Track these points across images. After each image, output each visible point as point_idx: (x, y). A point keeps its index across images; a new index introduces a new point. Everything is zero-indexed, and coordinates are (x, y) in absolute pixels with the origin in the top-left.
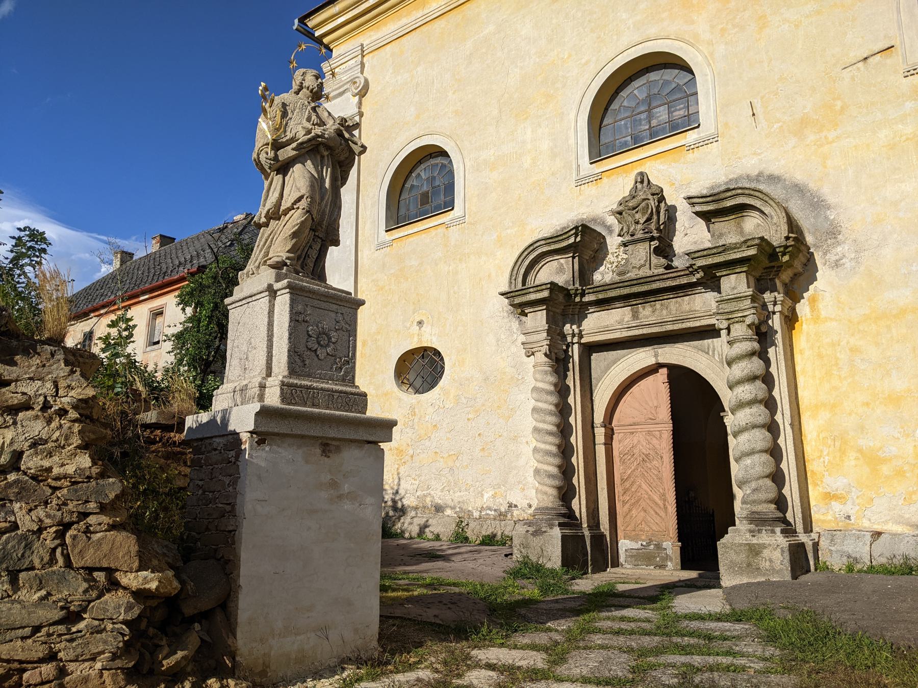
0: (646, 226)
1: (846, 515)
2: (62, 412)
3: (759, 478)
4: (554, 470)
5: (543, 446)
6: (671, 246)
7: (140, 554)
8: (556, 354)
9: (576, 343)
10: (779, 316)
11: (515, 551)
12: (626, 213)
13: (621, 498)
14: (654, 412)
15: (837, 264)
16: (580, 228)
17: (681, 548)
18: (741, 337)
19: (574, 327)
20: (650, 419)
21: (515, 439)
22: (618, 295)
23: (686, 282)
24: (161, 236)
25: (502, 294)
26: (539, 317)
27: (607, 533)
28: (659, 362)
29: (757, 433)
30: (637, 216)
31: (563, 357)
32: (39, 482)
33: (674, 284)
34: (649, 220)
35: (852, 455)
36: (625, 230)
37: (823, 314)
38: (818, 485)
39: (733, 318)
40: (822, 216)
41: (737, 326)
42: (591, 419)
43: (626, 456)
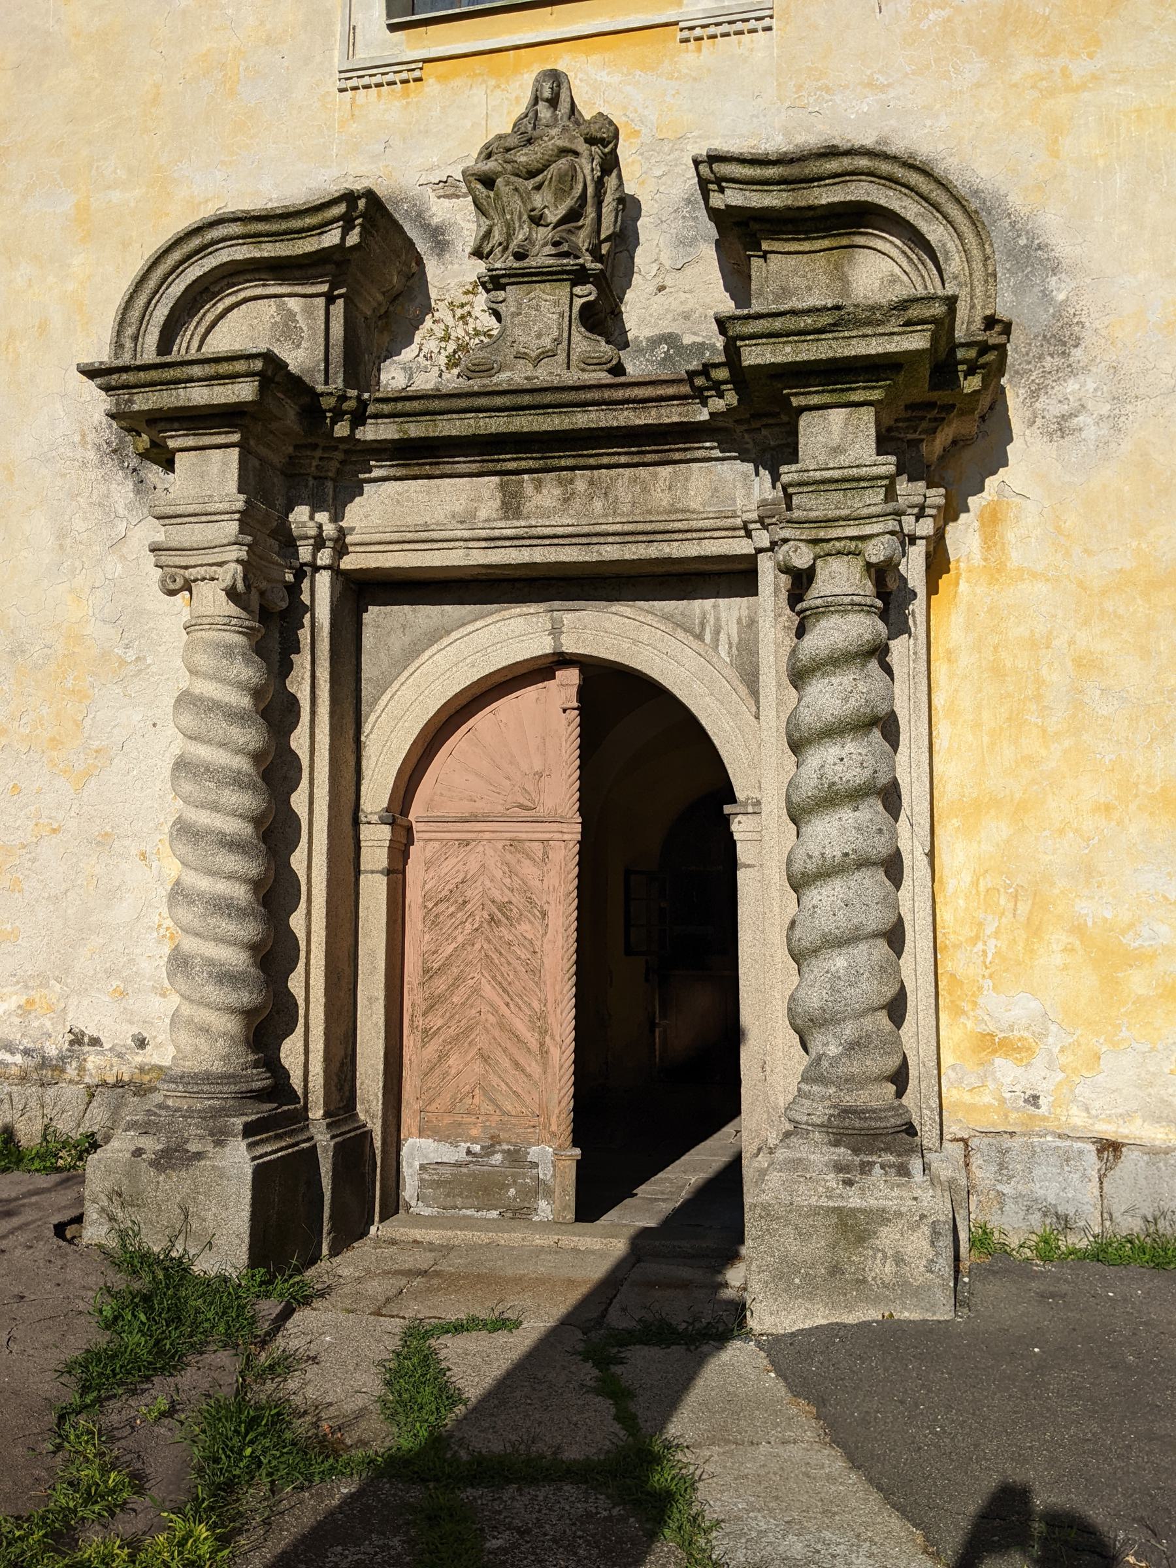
0: (564, 235)
1: (1029, 1092)
3: (865, 1013)
4: (236, 958)
5: (204, 884)
6: (617, 314)
8: (262, 594)
9: (325, 568)
10: (923, 549)
11: (92, 1213)
12: (508, 183)
13: (420, 1022)
14: (530, 787)
15: (1062, 428)
16: (361, 204)
17: (579, 1164)
18: (847, 600)
19: (322, 517)
20: (521, 806)
21: (103, 842)
22: (471, 432)
23: (675, 419)
25: (91, 373)
26: (214, 468)
27: (376, 1127)
28: (564, 649)
29: (868, 883)
30: (538, 200)
31: (284, 605)
33: (642, 422)
34: (573, 215)
35: (1058, 938)
36: (497, 236)
37: (1015, 558)
38: (964, 1012)
39: (828, 541)
40: (1036, 289)
41: (837, 565)
42: (353, 797)
43: (442, 907)
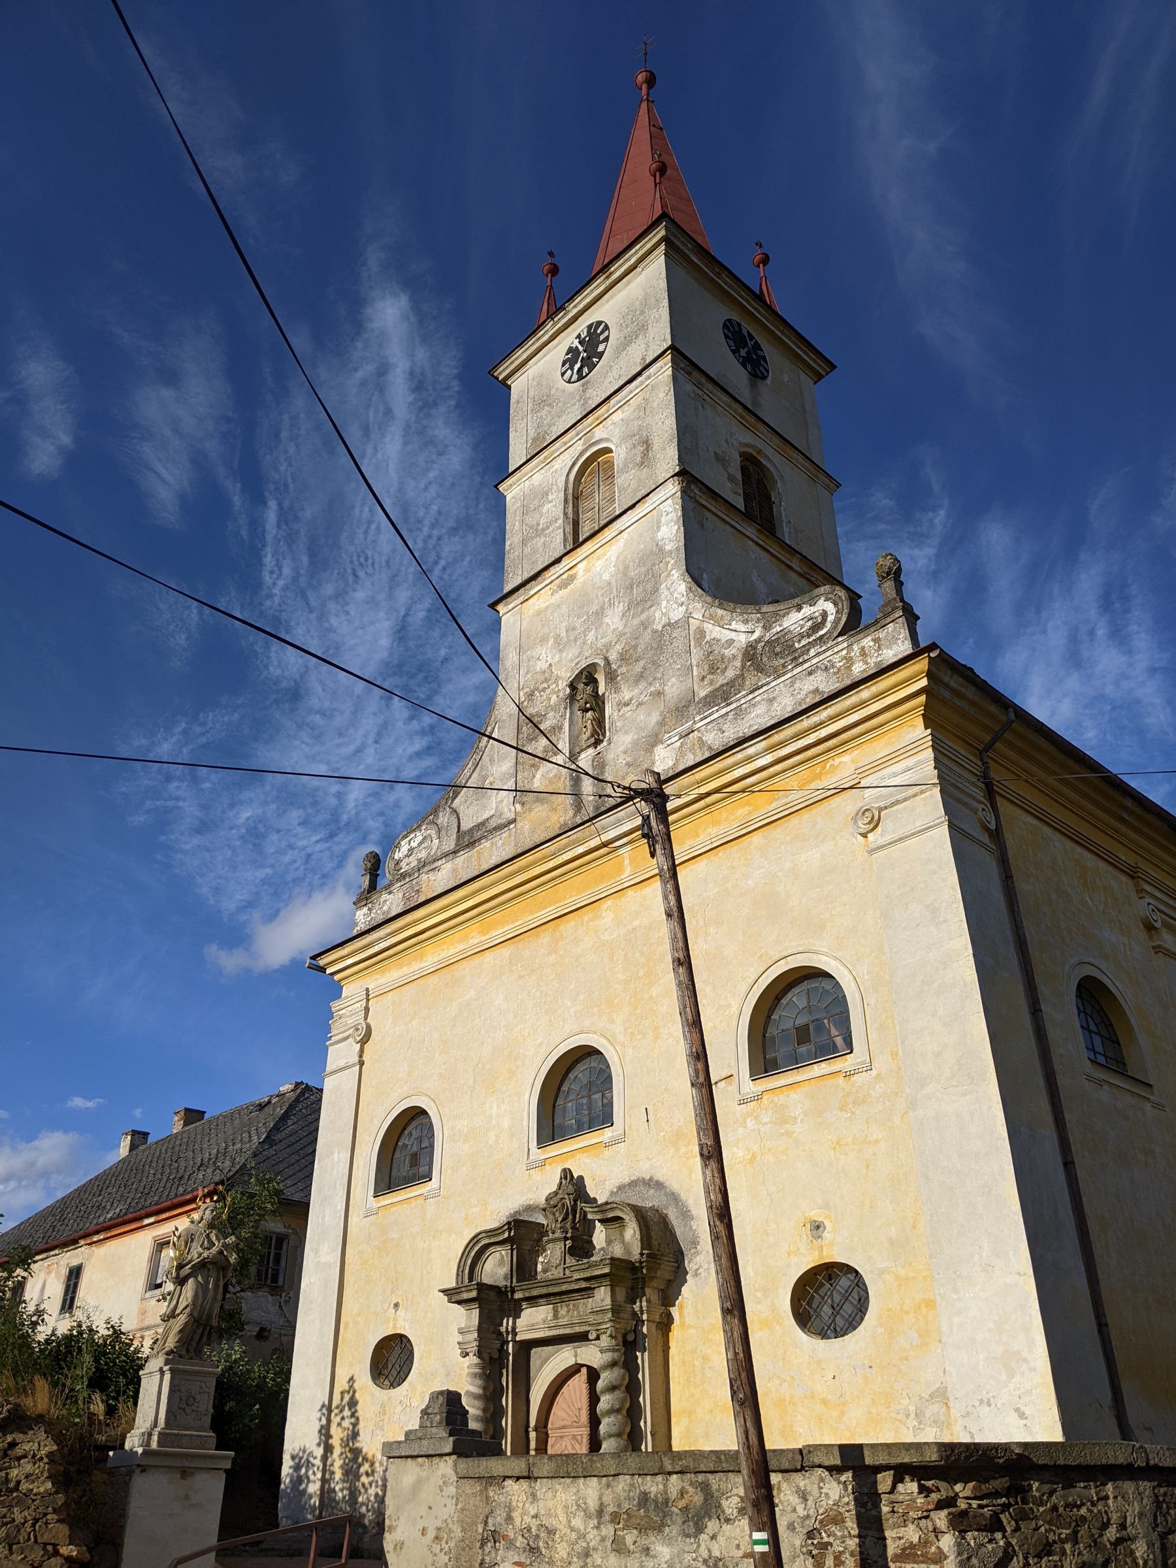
2: (41, 1459)
7: (70, 1537)
24: (186, 1109)
32: (27, 1496)
